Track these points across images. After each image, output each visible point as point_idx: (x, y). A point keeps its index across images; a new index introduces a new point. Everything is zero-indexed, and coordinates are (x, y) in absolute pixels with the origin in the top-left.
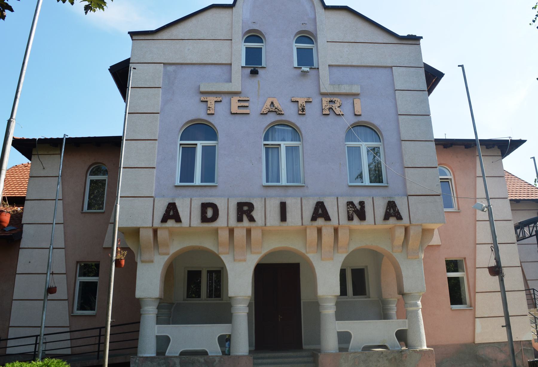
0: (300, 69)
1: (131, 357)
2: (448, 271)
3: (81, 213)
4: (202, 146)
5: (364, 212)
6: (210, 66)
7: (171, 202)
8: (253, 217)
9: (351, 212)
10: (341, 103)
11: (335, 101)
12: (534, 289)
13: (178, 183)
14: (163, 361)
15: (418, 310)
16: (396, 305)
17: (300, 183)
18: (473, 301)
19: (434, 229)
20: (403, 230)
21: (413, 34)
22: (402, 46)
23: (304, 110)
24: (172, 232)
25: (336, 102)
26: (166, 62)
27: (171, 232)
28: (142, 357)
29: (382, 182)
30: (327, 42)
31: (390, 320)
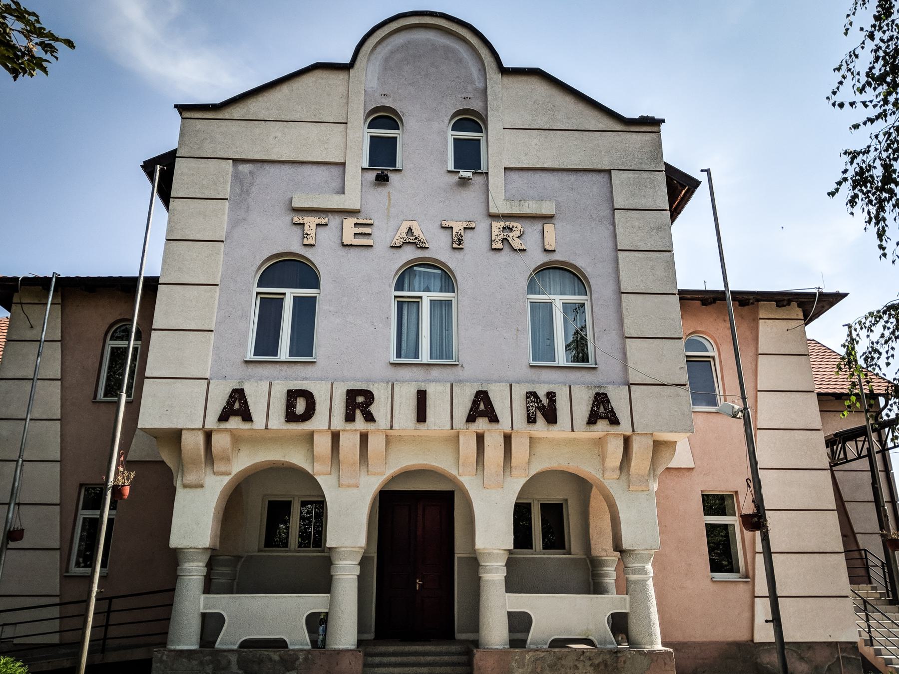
0: (457, 174)
1: (155, 650)
2: (707, 513)
3: (93, 402)
4: (294, 297)
6: (310, 165)
9: (532, 410)
10: (522, 231)
11: (513, 227)
12: (865, 551)
13: (250, 356)
15: (646, 581)
17: (452, 361)
18: (750, 568)
19: (676, 442)
20: (621, 443)
21: (650, 115)
22: (628, 135)
23: (462, 242)
24: (237, 439)
25: (514, 229)
26: (237, 157)
28: (174, 651)
30: (504, 128)
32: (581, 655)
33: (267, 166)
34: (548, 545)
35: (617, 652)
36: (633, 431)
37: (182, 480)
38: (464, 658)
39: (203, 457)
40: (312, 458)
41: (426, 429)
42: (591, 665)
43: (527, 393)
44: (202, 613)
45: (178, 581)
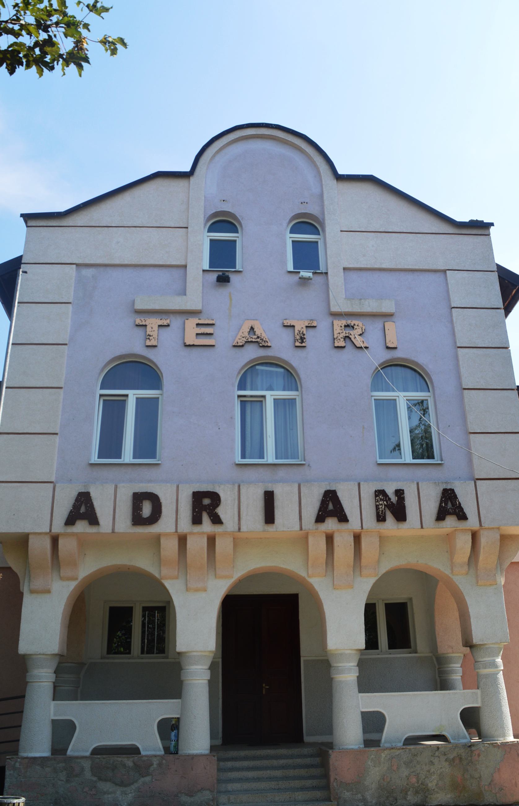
1: (8, 757)
6: (152, 268)
9: (382, 508)
10: (363, 329)
11: (354, 325)
13: (95, 458)
15: (497, 674)
17: (298, 460)
20: (468, 538)
23: (304, 340)
25: (355, 327)
28: (27, 758)
30: (341, 231)
32: (436, 751)
34: (392, 645)
35: (471, 746)
36: (481, 525)
37: (29, 585)
38: (318, 760)
39: (50, 561)
40: (159, 561)
41: (275, 530)
42: (446, 760)
44: (52, 720)
45: (28, 688)
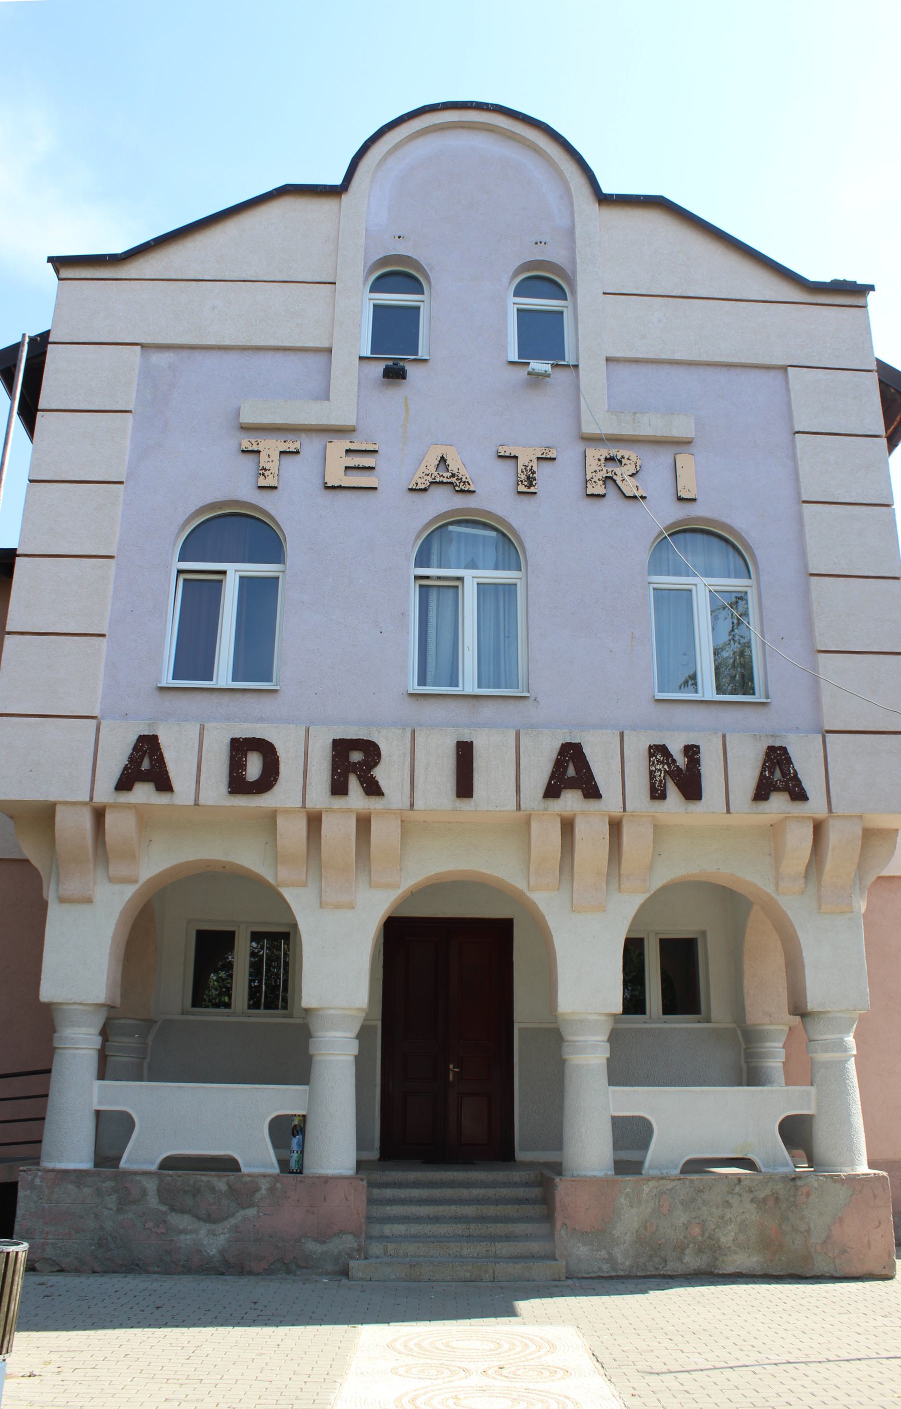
1: (21, 1168)
4: (241, 578)
5: (699, 776)
6: (271, 353)
7: (146, 733)
8: (377, 782)
11: (623, 457)
13: (167, 680)
14: (109, 1184)
15: (846, 1061)
16: (785, 1043)
17: (517, 690)
21: (849, 278)
25: (624, 461)
27: (142, 814)
28: (53, 1171)
29: (754, 694)
30: (604, 293)
31: (765, 1088)
32: (735, 1185)
33: (198, 355)
36: (830, 810)
37: (57, 890)
42: (752, 1201)
43: (650, 747)
